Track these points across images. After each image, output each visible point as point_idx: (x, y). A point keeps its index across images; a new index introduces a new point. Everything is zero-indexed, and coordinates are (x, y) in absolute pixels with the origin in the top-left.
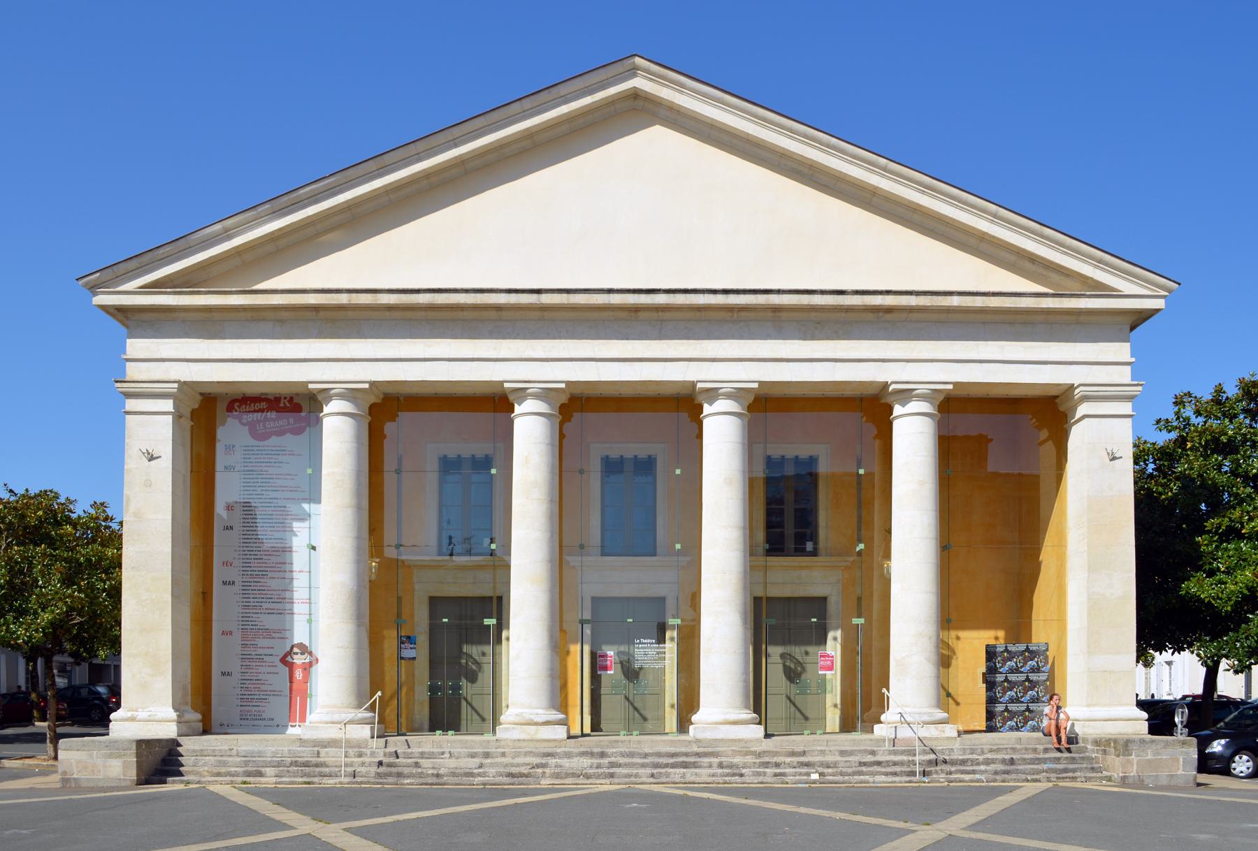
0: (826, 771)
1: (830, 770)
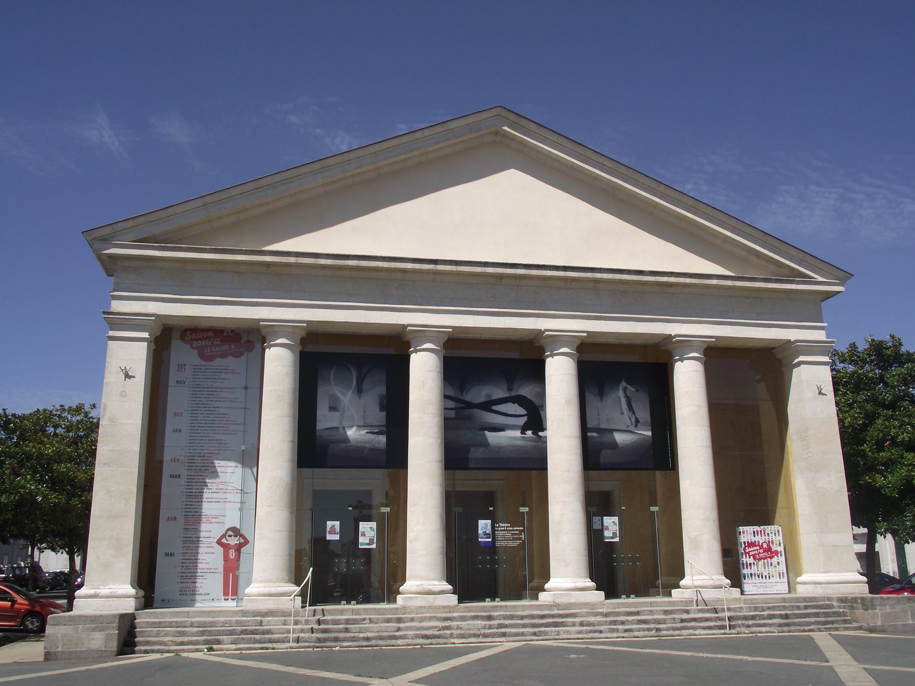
0: (661, 626)
1: (664, 626)
